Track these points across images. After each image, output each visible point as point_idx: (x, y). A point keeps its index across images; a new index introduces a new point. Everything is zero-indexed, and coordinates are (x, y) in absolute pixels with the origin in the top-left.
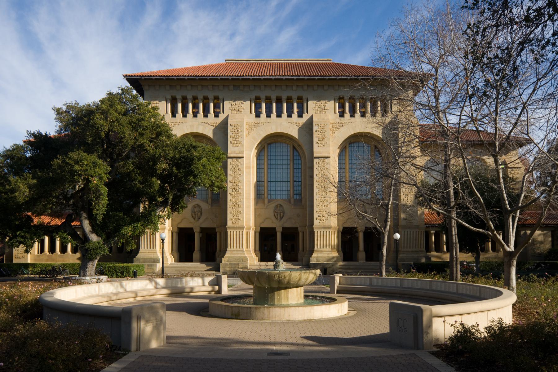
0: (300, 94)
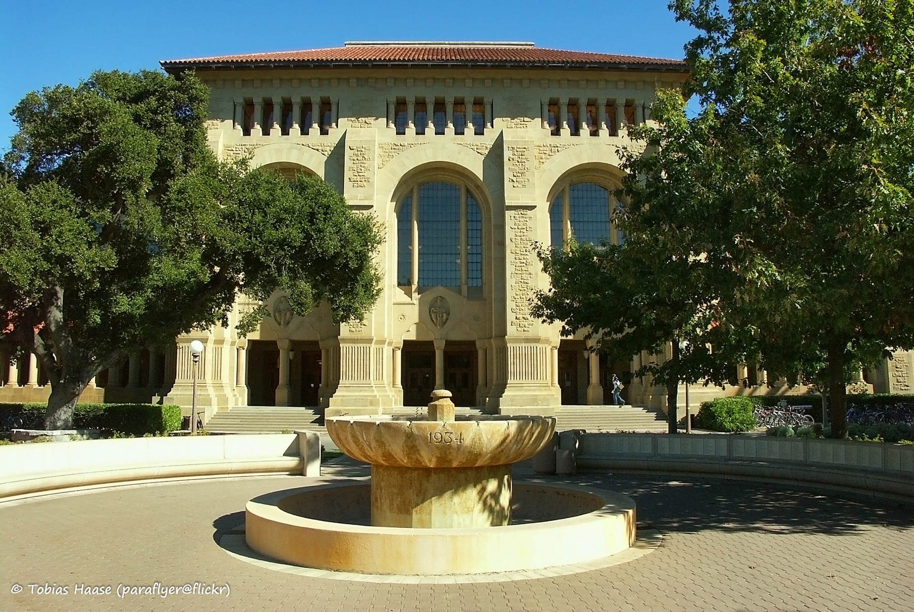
0: (479, 92)
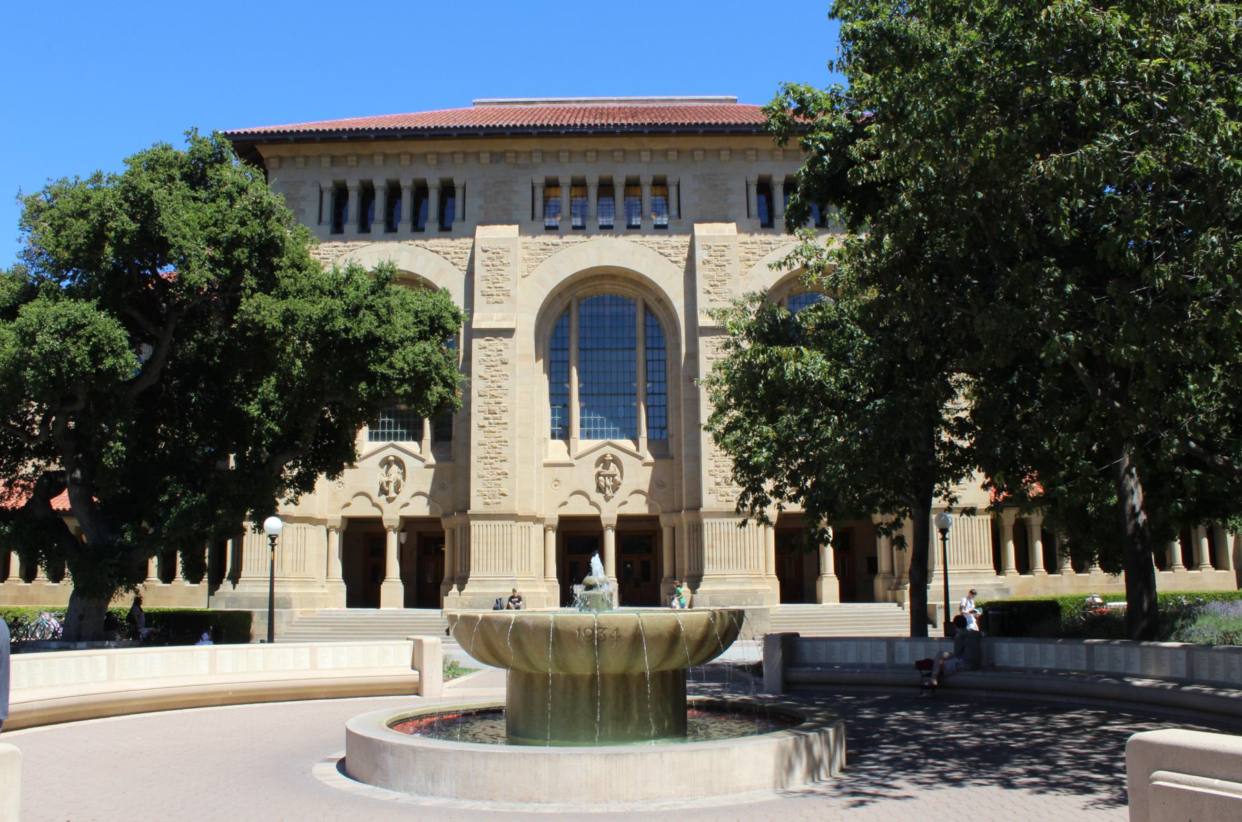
0: (660, 170)
